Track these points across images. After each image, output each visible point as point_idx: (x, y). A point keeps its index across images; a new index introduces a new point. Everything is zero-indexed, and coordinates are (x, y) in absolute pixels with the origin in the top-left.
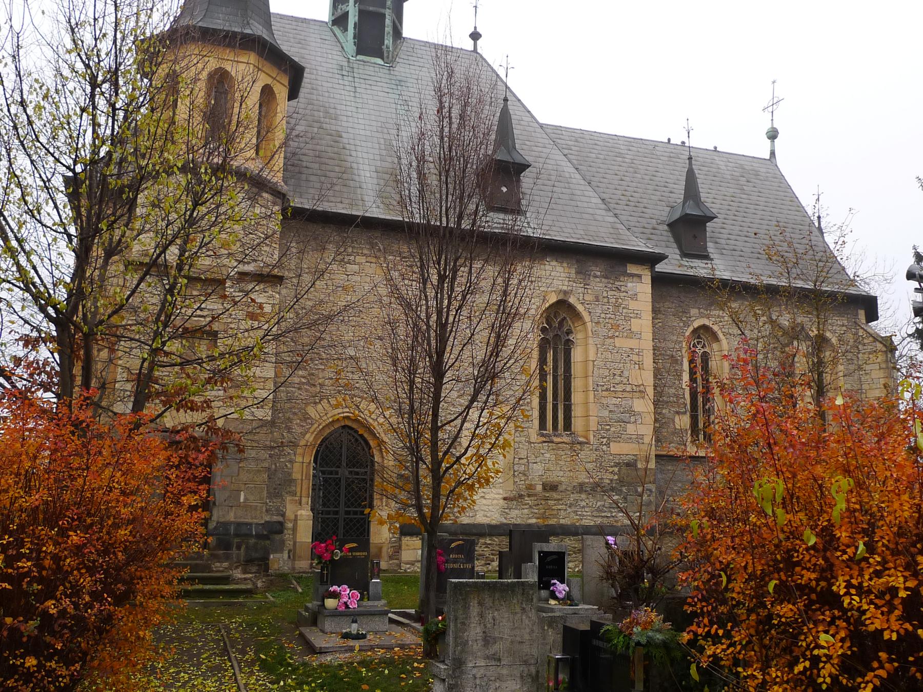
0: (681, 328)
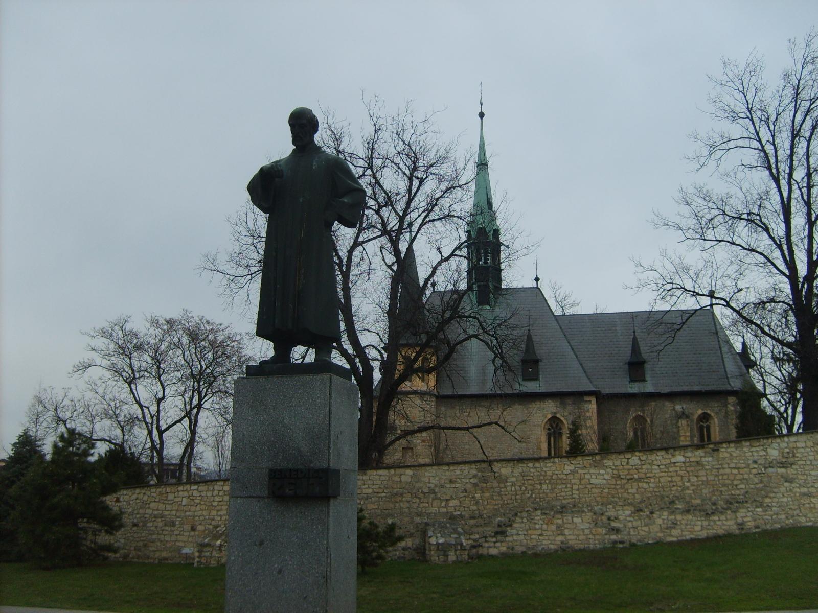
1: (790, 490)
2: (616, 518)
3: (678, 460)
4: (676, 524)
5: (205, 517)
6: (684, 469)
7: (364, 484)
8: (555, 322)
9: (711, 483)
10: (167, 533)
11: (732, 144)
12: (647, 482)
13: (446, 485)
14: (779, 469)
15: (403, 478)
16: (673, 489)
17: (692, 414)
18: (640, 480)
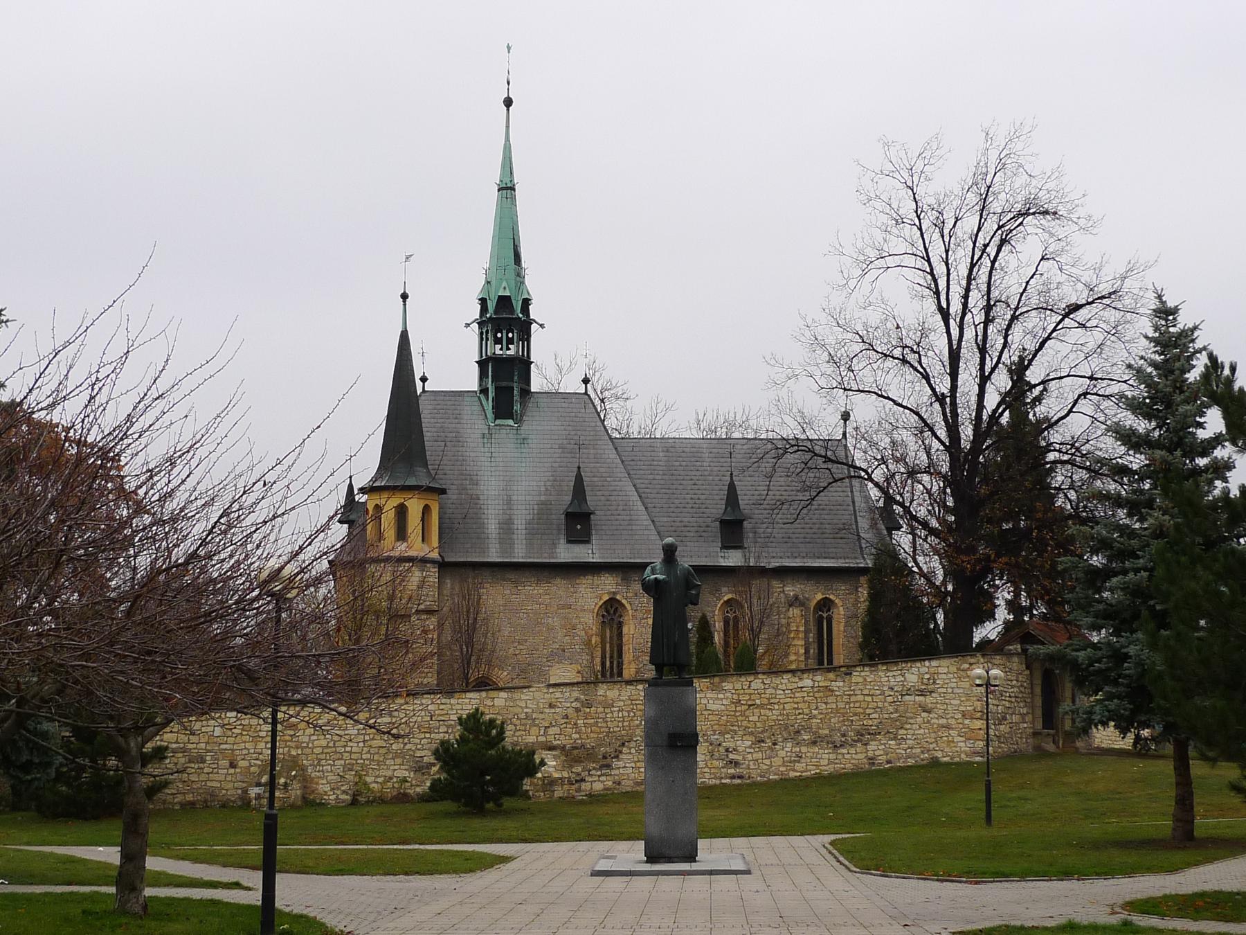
0: (714, 602)
1: (928, 720)
2: (734, 750)
3: (805, 685)
4: (801, 757)
5: (249, 750)
6: (811, 694)
7: (452, 709)
8: (614, 451)
9: (841, 711)
10: (193, 770)
11: (890, 261)
12: (770, 709)
13: (546, 710)
14: (917, 697)
15: (497, 702)
16: (798, 717)
17: (808, 599)
18: (762, 706)
